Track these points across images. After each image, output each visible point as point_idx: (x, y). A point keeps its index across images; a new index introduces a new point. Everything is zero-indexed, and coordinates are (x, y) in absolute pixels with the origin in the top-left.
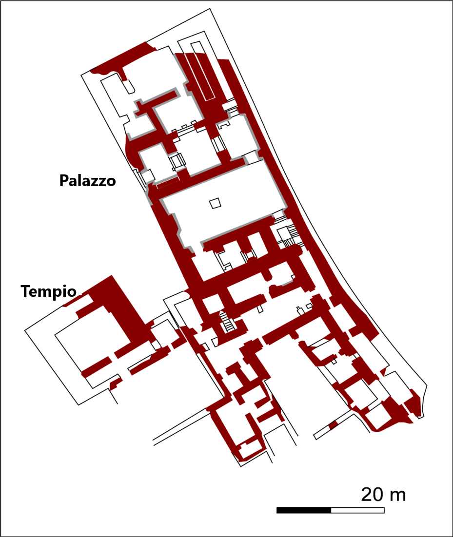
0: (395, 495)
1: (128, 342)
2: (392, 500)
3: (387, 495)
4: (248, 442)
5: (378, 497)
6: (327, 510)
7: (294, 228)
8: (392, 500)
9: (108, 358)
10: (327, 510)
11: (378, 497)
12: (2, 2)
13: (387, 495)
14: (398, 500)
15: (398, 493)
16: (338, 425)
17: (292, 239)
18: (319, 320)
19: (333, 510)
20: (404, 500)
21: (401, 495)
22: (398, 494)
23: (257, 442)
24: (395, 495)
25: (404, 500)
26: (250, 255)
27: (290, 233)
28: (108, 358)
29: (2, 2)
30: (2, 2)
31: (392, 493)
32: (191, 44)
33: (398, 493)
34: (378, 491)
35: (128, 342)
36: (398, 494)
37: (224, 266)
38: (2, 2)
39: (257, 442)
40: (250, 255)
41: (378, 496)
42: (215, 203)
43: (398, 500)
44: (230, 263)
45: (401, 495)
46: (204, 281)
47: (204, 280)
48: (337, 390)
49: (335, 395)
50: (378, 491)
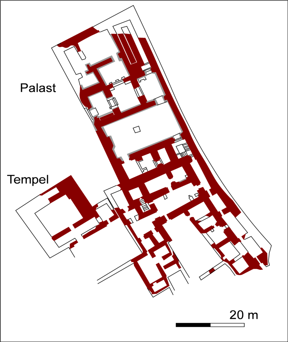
0: (251, 315)
1: (81, 218)
2: (249, 318)
3: (246, 315)
5: (240, 317)
6: (208, 325)
8: (249, 318)
10: (208, 325)
11: (240, 317)
12: (1, 1)
13: (246, 315)
19: (212, 325)
20: (257, 318)
21: (255, 315)
22: (253, 315)
24: (251, 315)
25: (257, 318)
29: (1, 1)
30: (1, 1)
31: (249, 314)
32: (121, 28)
34: (240, 313)
35: (81, 218)
36: (253, 315)
38: (1, 1)
41: (240, 316)
44: (146, 167)
45: (255, 315)
46: (130, 179)
47: (130, 178)
50: (240, 313)
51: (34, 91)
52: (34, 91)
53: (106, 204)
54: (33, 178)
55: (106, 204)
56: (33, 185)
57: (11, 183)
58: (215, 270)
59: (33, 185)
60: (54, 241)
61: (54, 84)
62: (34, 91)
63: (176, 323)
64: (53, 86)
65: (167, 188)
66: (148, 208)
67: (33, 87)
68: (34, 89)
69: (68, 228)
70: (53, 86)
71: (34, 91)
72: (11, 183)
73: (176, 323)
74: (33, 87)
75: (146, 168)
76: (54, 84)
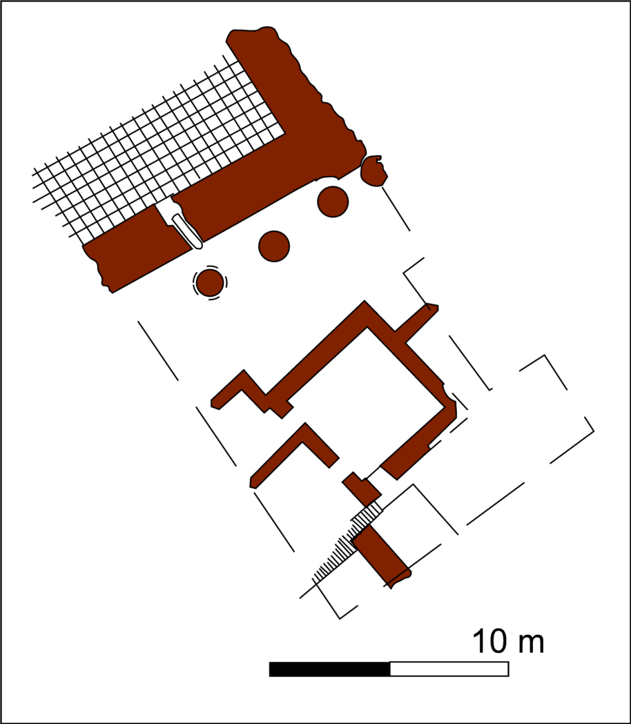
0: (526, 641)
2: (521, 651)
3: (513, 642)
5: (498, 646)
6: (381, 669)
7: (355, 535)
8: (521, 651)
10: (381, 669)
11: (498, 646)
12: (629, 722)
13: (513, 642)
14: (531, 651)
15: (532, 639)
16: (380, 466)
17: (366, 510)
19: (394, 669)
20: (542, 651)
21: (537, 641)
22: (533, 641)
24: (526, 641)
25: (542, 651)
27: (376, 517)
29: (629, 722)
30: (629, 722)
31: (522, 638)
33: (532, 639)
34: (498, 635)
36: (533, 641)
38: (629, 722)
41: (498, 645)
43: (531, 651)
45: (537, 641)
48: (431, 446)
49: (478, 630)
50: (498, 635)
53: (594, 431)
55: (594, 431)
63: (271, 664)
65: (212, 406)
66: (320, 578)
69: (345, 482)
73: (271, 664)
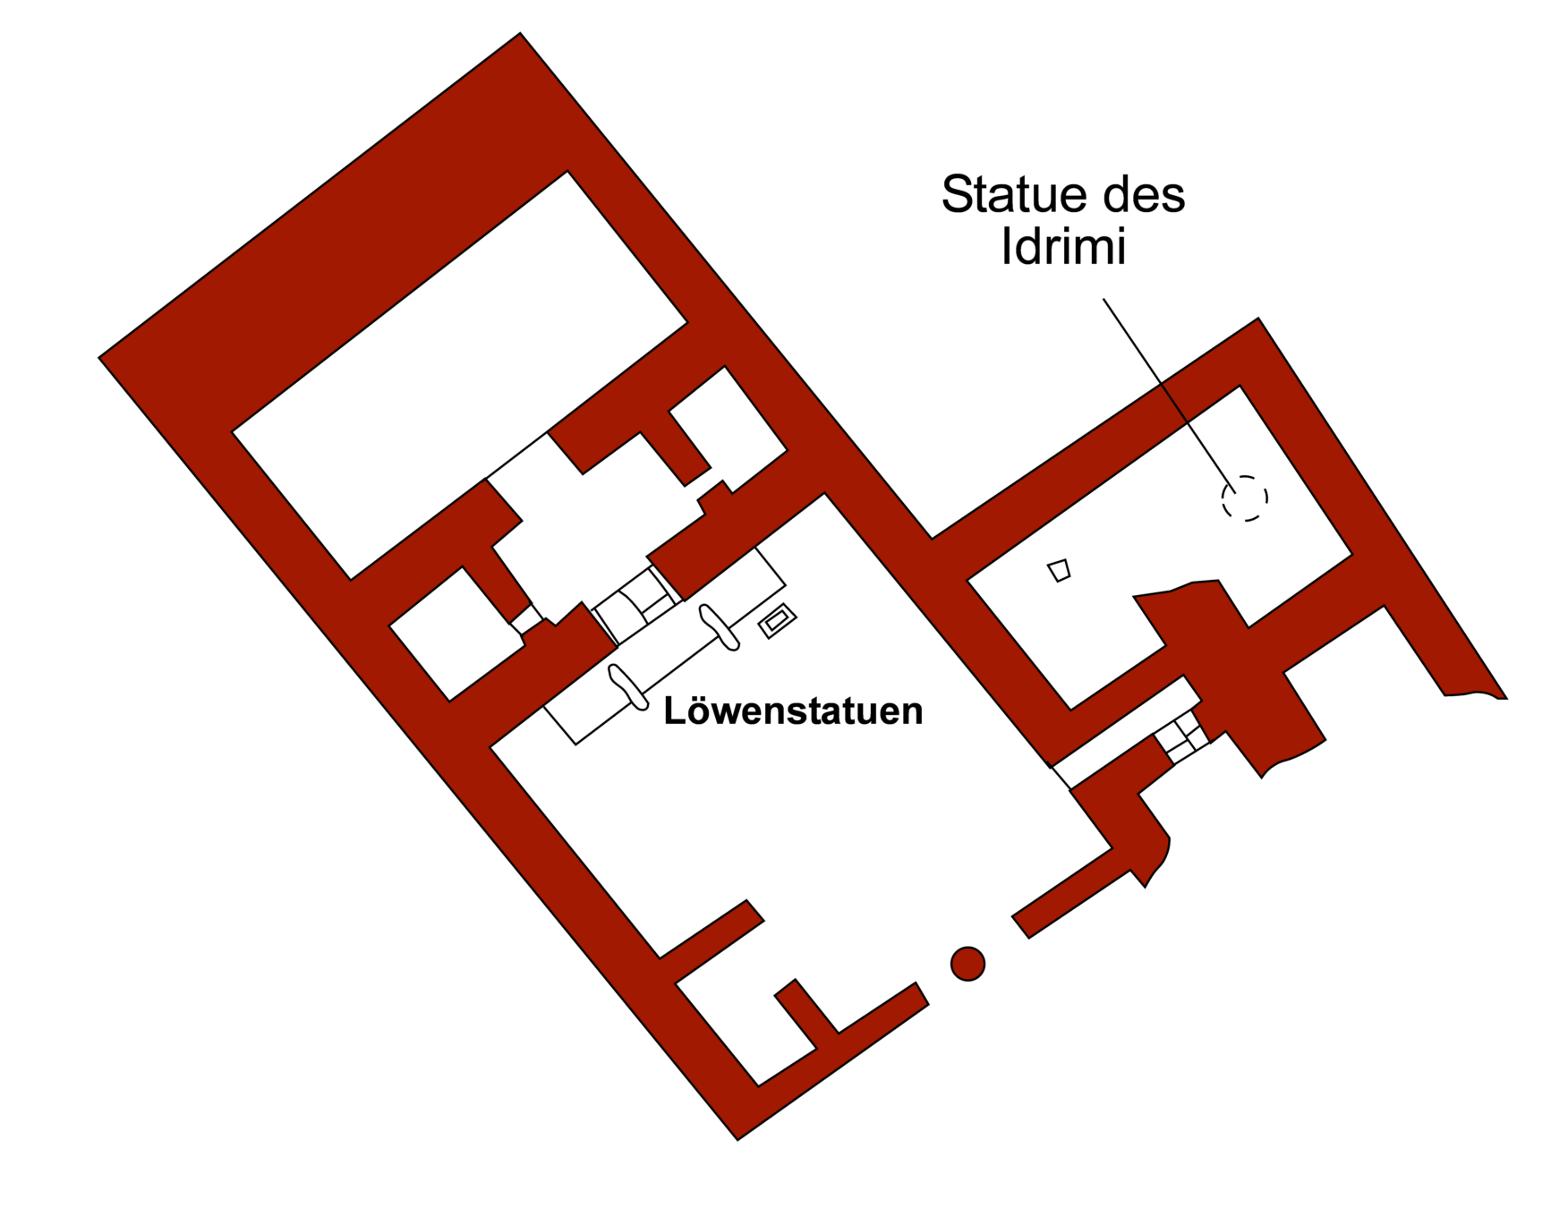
1: (565, 196)
4: (795, 1000)
9: (584, 461)
14: (1094, 261)
15: (1094, 243)
18: (935, 521)
23: (796, 1045)
26: (527, 620)
28: (584, 461)
32: (1049, 566)
33: (1094, 243)
35: (565, 196)
37: (787, 617)
39: (796, 1045)
40: (527, 620)
42: (1060, 570)
43: (1094, 261)
44: (759, 624)
46: (451, 689)
47: (451, 689)
51: (1010, 207)
52: (1010, 207)
54: (1037, 259)
56: (1037, 229)
57: (1007, 261)
58: (1174, 765)
59: (1037, 229)
60: (1177, 765)
61: (1022, 179)
62: (1011, 210)
64: (1018, 186)
67: (1004, 192)
68: (1010, 197)
70: (1018, 186)
71: (1011, 210)
72: (1007, 261)
74: (1004, 192)
75: (763, 624)
76: (1022, 179)
